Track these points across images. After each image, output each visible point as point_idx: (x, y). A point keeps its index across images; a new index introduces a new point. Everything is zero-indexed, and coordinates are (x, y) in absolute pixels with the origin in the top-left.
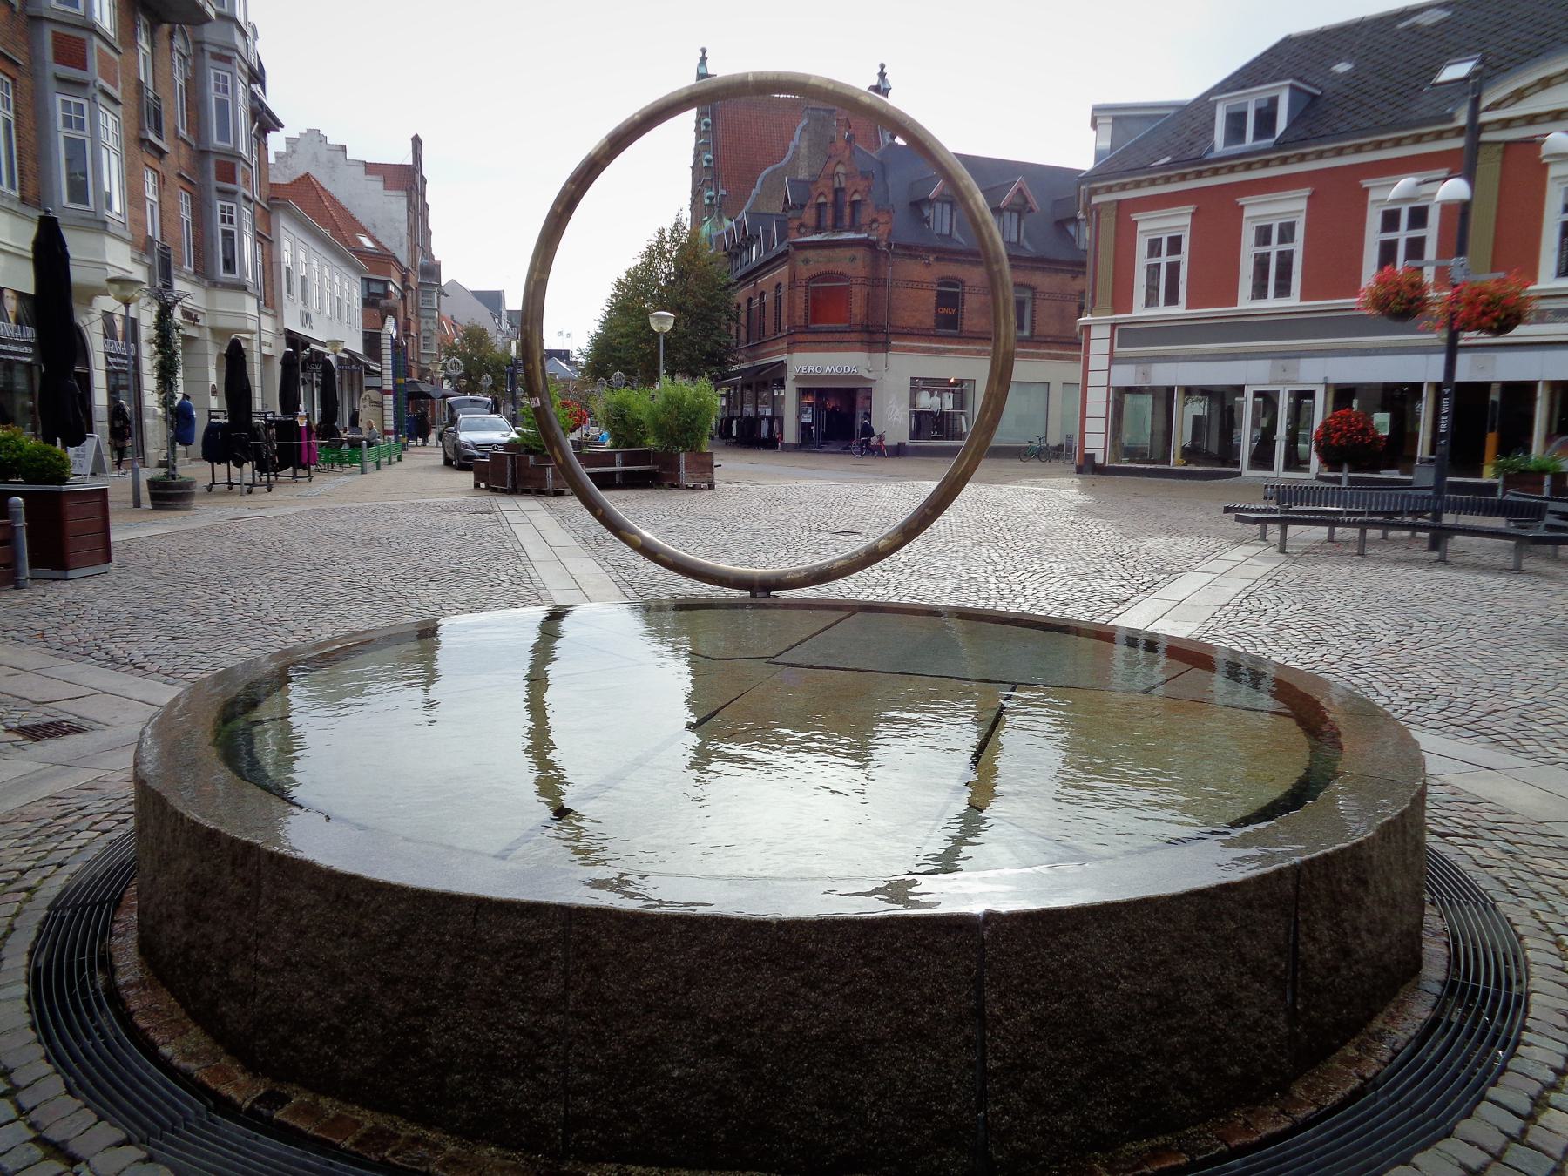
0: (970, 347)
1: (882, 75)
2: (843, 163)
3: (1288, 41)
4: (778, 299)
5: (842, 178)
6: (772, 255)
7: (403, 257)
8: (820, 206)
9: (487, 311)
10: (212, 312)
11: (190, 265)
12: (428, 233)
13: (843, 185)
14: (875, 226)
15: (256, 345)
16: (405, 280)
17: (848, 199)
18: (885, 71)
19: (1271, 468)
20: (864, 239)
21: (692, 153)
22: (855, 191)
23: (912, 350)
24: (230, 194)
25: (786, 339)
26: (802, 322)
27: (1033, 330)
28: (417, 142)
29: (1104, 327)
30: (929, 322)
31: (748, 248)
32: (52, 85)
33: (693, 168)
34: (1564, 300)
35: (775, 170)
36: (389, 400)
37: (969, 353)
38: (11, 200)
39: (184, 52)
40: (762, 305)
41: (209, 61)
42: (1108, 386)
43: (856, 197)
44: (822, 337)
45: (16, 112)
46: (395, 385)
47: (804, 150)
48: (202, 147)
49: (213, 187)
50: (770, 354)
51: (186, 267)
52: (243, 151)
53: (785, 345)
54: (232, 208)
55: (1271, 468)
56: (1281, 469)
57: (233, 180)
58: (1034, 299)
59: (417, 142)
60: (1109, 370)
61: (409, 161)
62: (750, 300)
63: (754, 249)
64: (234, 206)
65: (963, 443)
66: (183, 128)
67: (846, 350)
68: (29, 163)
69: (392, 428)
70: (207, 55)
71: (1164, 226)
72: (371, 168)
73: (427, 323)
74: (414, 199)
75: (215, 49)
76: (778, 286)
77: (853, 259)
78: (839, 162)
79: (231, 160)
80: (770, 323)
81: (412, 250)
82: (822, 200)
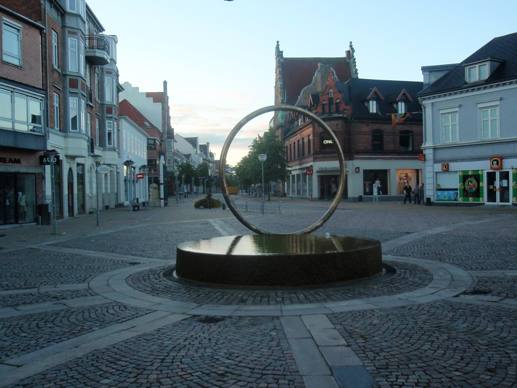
0: (387, 156)
1: (351, 46)
2: (332, 88)
3: (496, 38)
4: (309, 140)
5: (332, 94)
6: (306, 124)
7: (160, 129)
8: (324, 105)
9: (191, 146)
10: (67, 148)
11: (57, 127)
12: (169, 118)
13: (332, 97)
14: (346, 111)
15: (115, 168)
16: (161, 137)
17: (334, 102)
18: (352, 44)
19: (495, 201)
20: (341, 117)
21: (275, 81)
22: (337, 99)
23: (363, 159)
24: (110, 118)
25: (312, 156)
26: (318, 150)
27: (413, 148)
28: (165, 83)
29: (430, 150)
30: (370, 148)
31: (297, 120)
32: (68, 94)
33: (275, 87)
34: (511, 145)
35: (308, 88)
36: (162, 187)
37: (387, 159)
38: (57, 130)
39: (98, 73)
40: (303, 143)
41: (105, 74)
42: (433, 172)
43: (338, 101)
44: (327, 156)
45: (59, 105)
46: (164, 181)
47: (319, 79)
48: (64, 73)
49: (105, 116)
50: (307, 162)
51: (56, 128)
52: (82, 73)
53: (312, 159)
54: (111, 123)
55: (495, 201)
56: (499, 201)
57: (111, 113)
58: (413, 136)
59: (165, 83)
60: (433, 166)
61: (162, 91)
62: (299, 141)
63: (300, 120)
64: (112, 122)
65: (498, 202)
66: (56, 65)
67: (328, 160)
68: (62, 119)
69: (163, 197)
70: (105, 72)
71: (451, 109)
72: (149, 95)
73: (169, 154)
74: (164, 105)
75: (107, 70)
76: (309, 135)
77: (337, 125)
78: (330, 88)
79: (111, 106)
80: (306, 150)
81: (164, 126)
82: (324, 102)
